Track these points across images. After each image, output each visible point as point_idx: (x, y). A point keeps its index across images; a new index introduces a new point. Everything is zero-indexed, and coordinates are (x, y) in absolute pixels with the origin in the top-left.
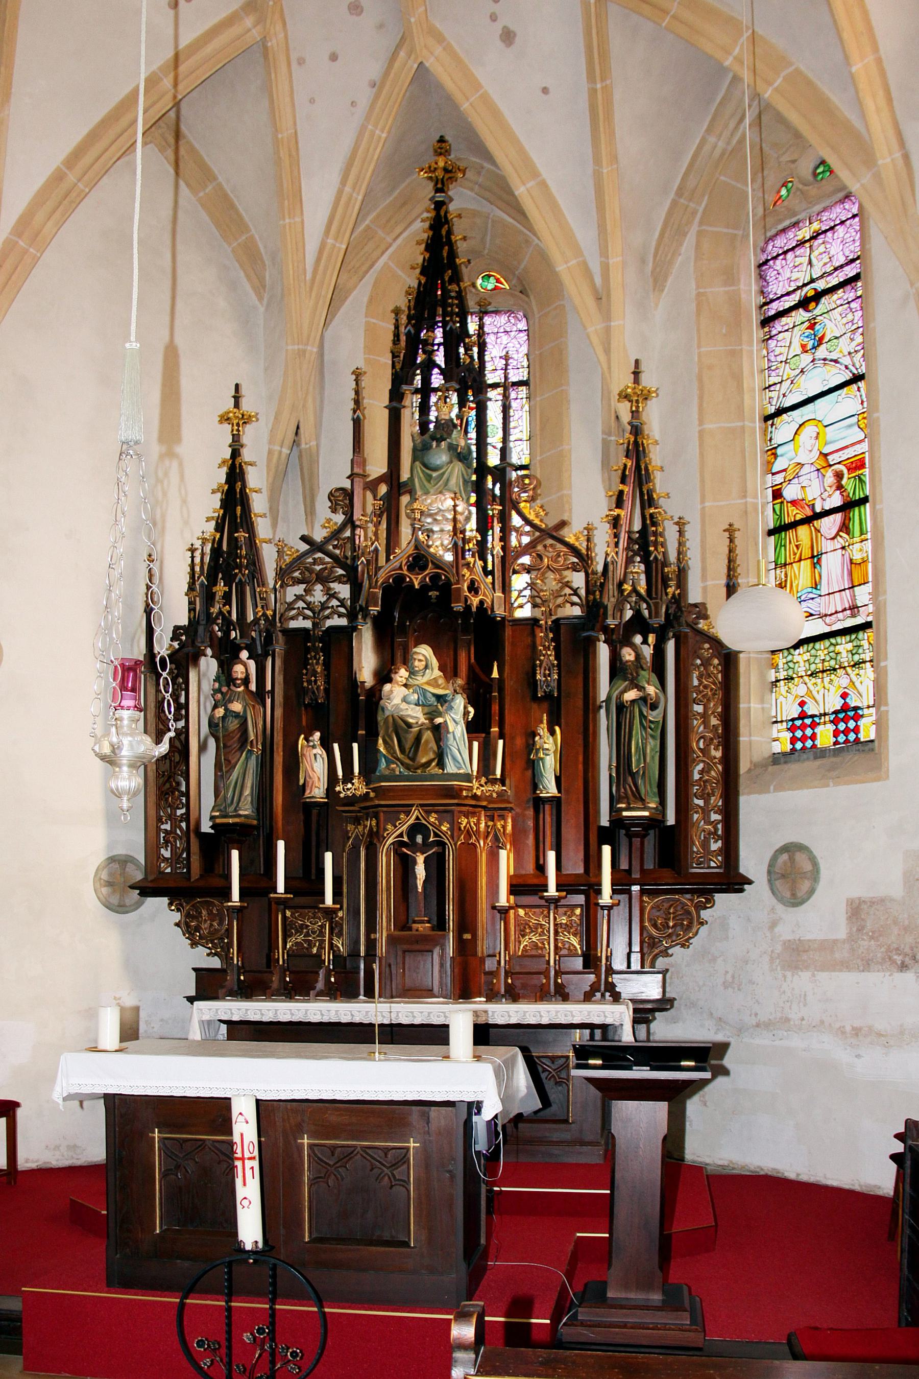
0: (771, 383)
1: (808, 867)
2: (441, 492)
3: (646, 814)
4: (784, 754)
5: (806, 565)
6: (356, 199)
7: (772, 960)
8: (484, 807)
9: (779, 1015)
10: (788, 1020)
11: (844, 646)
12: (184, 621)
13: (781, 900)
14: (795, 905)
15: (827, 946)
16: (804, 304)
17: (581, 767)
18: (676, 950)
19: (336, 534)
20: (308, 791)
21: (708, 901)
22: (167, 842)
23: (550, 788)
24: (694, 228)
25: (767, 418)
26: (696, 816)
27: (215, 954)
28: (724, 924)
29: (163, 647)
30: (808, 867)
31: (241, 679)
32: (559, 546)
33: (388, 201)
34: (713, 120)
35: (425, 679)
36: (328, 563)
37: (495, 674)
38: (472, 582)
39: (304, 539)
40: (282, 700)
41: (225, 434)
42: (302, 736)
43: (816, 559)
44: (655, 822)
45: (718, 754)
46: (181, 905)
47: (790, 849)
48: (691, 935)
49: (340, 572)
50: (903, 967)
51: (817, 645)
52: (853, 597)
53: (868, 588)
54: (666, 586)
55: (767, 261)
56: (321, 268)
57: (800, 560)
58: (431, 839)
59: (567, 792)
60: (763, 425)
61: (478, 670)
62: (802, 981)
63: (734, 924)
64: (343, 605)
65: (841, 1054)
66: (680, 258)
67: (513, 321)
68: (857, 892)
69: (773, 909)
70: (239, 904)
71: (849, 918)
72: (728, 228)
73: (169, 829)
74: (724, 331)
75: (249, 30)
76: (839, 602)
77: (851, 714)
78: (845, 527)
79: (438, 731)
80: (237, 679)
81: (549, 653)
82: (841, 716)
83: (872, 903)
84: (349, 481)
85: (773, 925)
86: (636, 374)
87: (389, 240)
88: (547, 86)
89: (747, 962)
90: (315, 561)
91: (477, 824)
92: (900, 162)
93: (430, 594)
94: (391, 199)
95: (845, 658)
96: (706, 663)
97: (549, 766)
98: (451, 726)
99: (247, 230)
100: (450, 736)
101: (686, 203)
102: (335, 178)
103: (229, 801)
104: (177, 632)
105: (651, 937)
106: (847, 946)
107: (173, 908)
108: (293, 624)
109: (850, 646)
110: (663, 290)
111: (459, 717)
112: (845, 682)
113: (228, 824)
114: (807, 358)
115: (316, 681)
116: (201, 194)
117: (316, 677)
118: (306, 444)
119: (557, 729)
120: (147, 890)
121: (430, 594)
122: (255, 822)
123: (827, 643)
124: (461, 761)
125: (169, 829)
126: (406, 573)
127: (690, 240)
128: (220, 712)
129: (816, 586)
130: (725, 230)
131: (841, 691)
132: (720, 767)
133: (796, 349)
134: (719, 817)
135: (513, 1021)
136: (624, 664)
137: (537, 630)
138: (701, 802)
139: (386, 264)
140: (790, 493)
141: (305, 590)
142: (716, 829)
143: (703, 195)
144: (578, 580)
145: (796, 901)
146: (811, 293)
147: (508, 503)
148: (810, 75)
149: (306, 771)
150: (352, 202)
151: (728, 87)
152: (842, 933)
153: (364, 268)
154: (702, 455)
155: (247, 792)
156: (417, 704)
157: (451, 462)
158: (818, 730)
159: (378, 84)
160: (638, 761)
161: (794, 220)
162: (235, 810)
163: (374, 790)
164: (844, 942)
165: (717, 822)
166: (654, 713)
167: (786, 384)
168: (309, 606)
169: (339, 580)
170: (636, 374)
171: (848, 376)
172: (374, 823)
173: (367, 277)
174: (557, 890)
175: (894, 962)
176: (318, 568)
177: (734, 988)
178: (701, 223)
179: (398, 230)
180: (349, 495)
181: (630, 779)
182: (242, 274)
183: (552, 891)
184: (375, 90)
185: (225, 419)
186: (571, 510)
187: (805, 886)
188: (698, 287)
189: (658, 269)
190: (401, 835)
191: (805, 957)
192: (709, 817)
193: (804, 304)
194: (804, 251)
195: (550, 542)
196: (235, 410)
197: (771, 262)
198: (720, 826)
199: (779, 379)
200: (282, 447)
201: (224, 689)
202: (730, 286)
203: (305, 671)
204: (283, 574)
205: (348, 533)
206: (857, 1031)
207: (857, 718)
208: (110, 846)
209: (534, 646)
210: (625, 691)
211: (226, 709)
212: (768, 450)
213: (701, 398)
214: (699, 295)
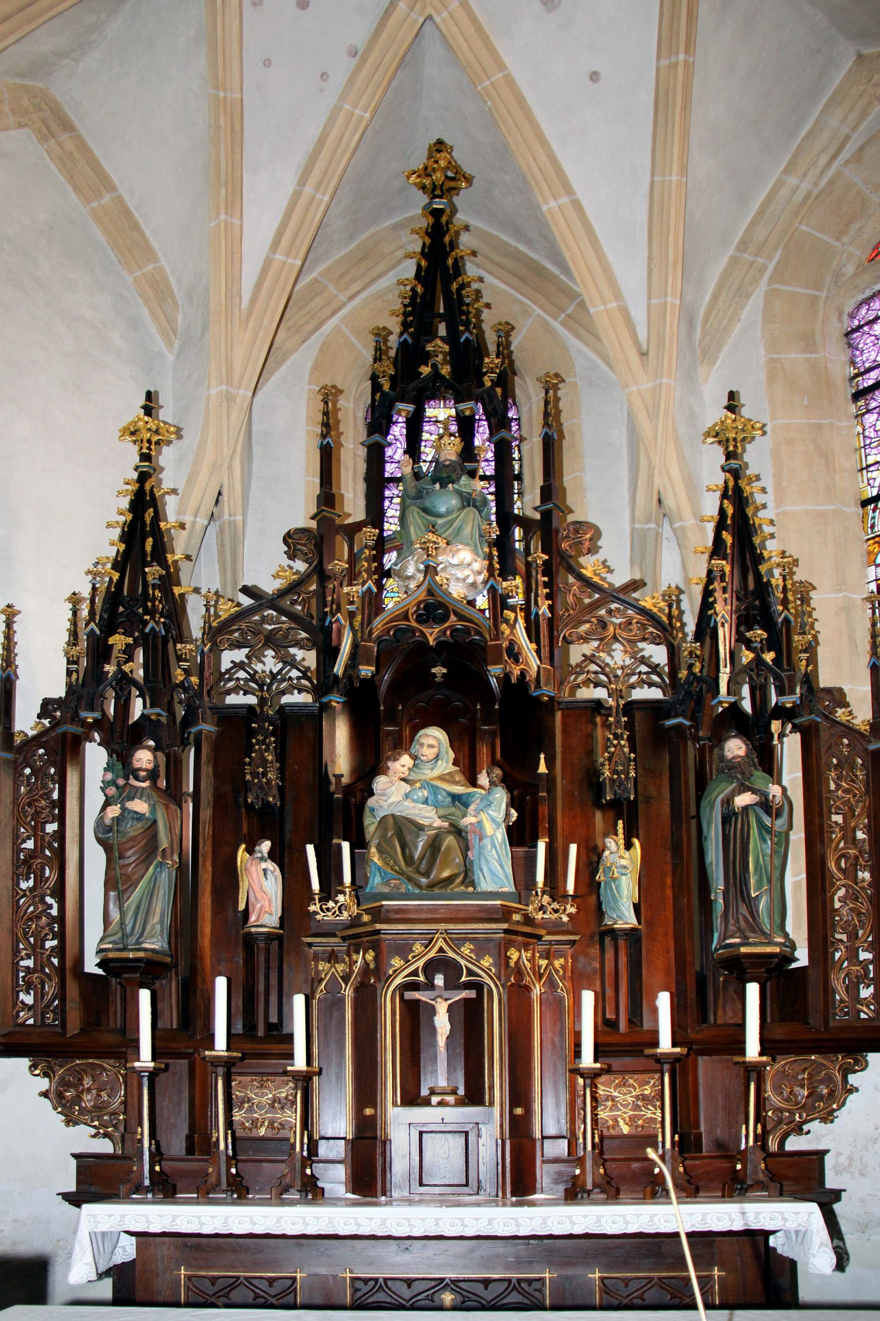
0: (869, 462)
6: (321, 200)
12: (59, 691)
19: (293, 588)
20: (253, 918)
21: (857, 1062)
24: (763, 286)
25: (865, 503)
27: (106, 1135)
31: (146, 770)
33: (342, 253)
34: (796, 155)
35: (437, 772)
36: (283, 623)
37: (542, 769)
40: (211, 798)
41: (131, 455)
42: (243, 846)
46: (52, 1069)
48: (835, 1106)
49: (304, 635)
55: (860, 327)
56: (264, 292)
58: (463, 979)
59: (650, 924)
60: (860, 511)
64: (305, 676)
66: (739, 325)
70: (226, 1054)
72: (807, 287)
73: (32, 966)
74: (806, 402)
80: (140, 769)
81: (623, 742)
87: (343, 297)
88: (599, 70)
90: (264, 620)
93: (434, 670)
94: (347, 251)
98: (489, 828)
100: (487, 842)
101: (751, 258)
103: (128, 929)
104: (47, 707)
107: (37, 1072)
110: (714, 363)
113: (128, 960)
115: (264, 774)
116: (95, 204)
117: (265, 768)
118: (230, 515)
119: (636, 842)
121: (434, 670)
122: (168, 960)
124: (502, 876)
125: (32, 966)
126: (414, 624)
127: (756, 302)
128: (114, 811)
130: (803, 291)
134: (869, 956)
135: (578, 1230)
141: (247, 657)
142: (867, 972)
143: (775, 249)
150: (315, 205)
151: (822, 112)
153: (309, 328)
155: (155, 919)
156: (426, 802)
159: (360, 53)
162: (138, 942)
163: (368, 911)
165: (867, 962)
168: (253, 677)
169: (298, 644)
172: (370, 955)
173: (313, 338)
177: (852, 1173)
178: (771, 280)
179: (354, 288)
182: (146, 312)
184: (354, 61)
189: (708, 338)
190: (415, 973)
192: (857, 955)
196: (146, 418)
197: (866, 328)
198: (871, 967)
200: (196, 516)
201: (121, 782)
202: (812, 352)
203: (247, 760)
211: (123, 809)
212: (868, 540)
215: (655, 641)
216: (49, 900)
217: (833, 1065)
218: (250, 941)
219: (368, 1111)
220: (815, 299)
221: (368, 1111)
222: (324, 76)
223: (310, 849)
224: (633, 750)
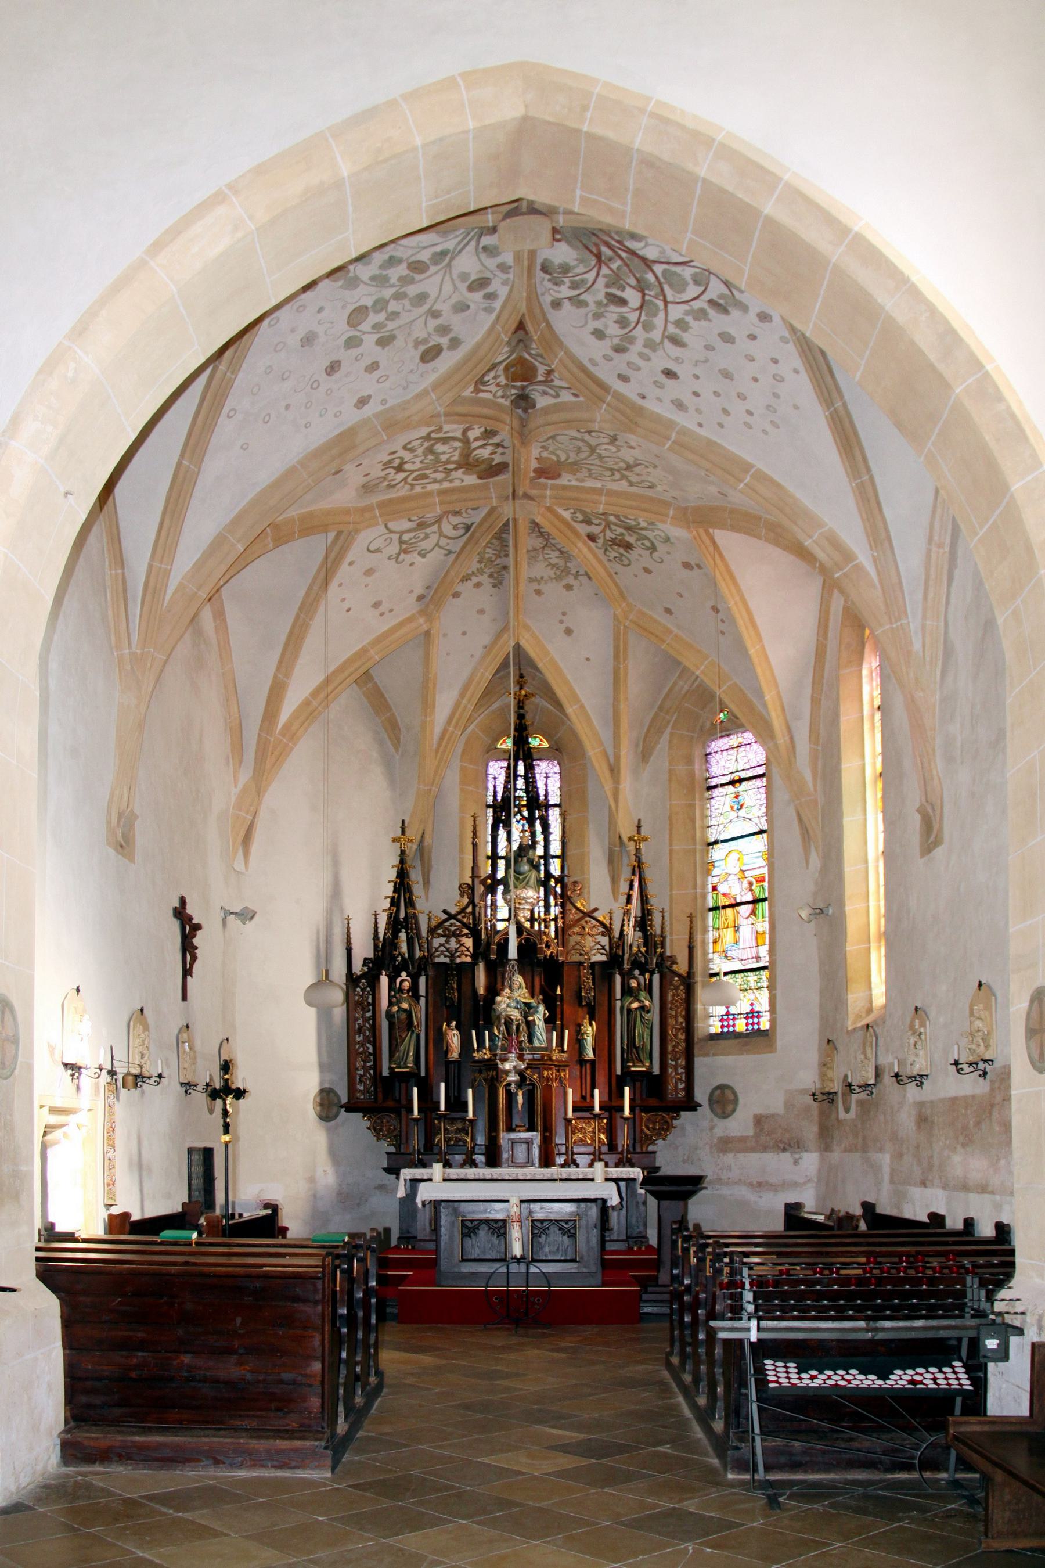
1: (732, 1097)
2: (524, 888)
3: (644, 1069)
4: (717, 1034)
5: (731, 930)
7: (711, 1147)
8: (555, 1065)
9: (715, 1177)
10: (720, 1179)
11: (752, 977)
13: (716, 1115)
14: (724, 1118)
15: (743, 1139)
16: (732, 783)
17: (606, 1043)
18: (660, 1142)
22: (361, 1081)
23: (590, 1054)
26: (670, 1070)
27: (393, 1145)
28: (683, 1129)
29: (358, 968)
30: (732, 1097)
32: (593, 921)
38: (547, 942)
39: (445, 911)
43: (736, 928)
44: (648, 1074)
45: (683, 1037)
47: (722, 1087)
49: (466, 931)
50: (784, 1150)
51: (737, 975)
52: (758, 952)
53: (767, 947)
54: (656, 948)
57: (727, 927)
61: (546, 988)
62: (729, 1158)
63: (689, 1129)
65: (750, 1196)
67: (551, 766)
68: (759, 1111)
69: (712, 1120)
71: (755, 1125)
75: (421, 625)
76: (750, 953)
77: (756, 1015)
78: (753, 913)
79: (530, 1025)
82: (750, 1015)
83: (767, 1117)
84: (471, 880)
85: (712, 1128)
86: (639, 827)
89: (696, 1149)
90: (452, 925)
91: (552, 1074)
92: (788, 741)
95: (752, 984)
96: (677, 988)
97: (589, 1042)
99: (391, 709)
100: (536, 1027)
102: (455, 693)
105: (647, 1135)
106: (754, 1140)
108: (437, 960)
109: (756, 978)
111: (541, 1017)
112: (752, 997)
114: (733, 815)
119: (594, 1023)
120: (350, 1108)
123: (742, 975)
128: (395, 1009)
129: (736, 942)
131: (750, 1002)
132: (684, 1044)
133: (727, 808)
134: (683, 1071)
136: (630, 988)
137: (582, 968)
138: (673, 1063)
139: (473, 730)
140: (722, 889)
144: (605, 941)
145: (725, 1115)
146: (737, 778)
147: (566, 898)
148: (742, 687)
149: (448, 1042)
152: (751, 1132)
154: (671, 863)
155: (411, 1054)
157: (530, 870)
158: (737, 1022)
160: (639, 1041)
161: (728, 733)
164: (752, 1137)
165: (682, 1073)
166: (648, 1015)
167: (721, 827)
168: (448, 950)
169: (466, 935)
170: (639, 827)
171: (757, 830)
172: (494, 1073)
174: (600, 1110)
175: (779, 1147)
176: (453, 929)
178: (673, 728)
179: (480, 712)
180: (472, 888)
181: (634, 1050)
182: (386, 736)
183: (597, 1109)
185: (395, 840)
186: (589, 887)
187: (730, 1107)
188: (670, 765)
191: (730, 1145)
193: (732, 783)
194: (733, 752)
195: (588, 919)
198: (684, 1076)
199: (717, 823)
204: (432, 931)
205: (470, 909)
206: (759, 1184)
207: (759, 1017)
208: (321, 1083)
209: (580, 977)
210: (631, 1003)
213: (671, 830)
214: (670, 770)
215: (603, 934)
216: (368, 1045)
217: (500, 1072)
218: (448, 1063)
219: (494, 1134)
220: (692, 737)
221: (494, 1134)
222: (472, 656)
223: (474, 1032)
224: (594, 984)
